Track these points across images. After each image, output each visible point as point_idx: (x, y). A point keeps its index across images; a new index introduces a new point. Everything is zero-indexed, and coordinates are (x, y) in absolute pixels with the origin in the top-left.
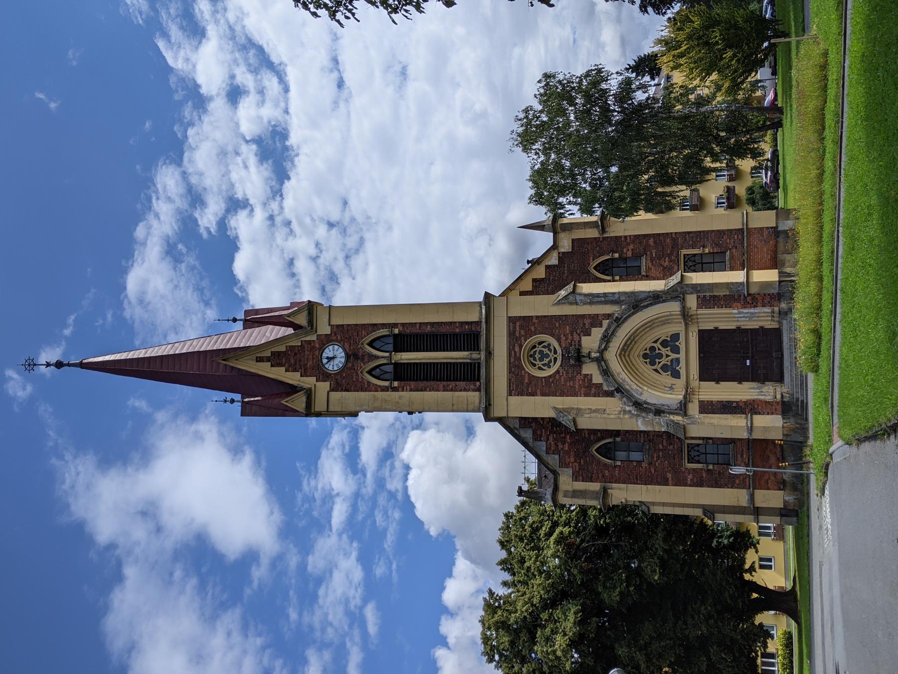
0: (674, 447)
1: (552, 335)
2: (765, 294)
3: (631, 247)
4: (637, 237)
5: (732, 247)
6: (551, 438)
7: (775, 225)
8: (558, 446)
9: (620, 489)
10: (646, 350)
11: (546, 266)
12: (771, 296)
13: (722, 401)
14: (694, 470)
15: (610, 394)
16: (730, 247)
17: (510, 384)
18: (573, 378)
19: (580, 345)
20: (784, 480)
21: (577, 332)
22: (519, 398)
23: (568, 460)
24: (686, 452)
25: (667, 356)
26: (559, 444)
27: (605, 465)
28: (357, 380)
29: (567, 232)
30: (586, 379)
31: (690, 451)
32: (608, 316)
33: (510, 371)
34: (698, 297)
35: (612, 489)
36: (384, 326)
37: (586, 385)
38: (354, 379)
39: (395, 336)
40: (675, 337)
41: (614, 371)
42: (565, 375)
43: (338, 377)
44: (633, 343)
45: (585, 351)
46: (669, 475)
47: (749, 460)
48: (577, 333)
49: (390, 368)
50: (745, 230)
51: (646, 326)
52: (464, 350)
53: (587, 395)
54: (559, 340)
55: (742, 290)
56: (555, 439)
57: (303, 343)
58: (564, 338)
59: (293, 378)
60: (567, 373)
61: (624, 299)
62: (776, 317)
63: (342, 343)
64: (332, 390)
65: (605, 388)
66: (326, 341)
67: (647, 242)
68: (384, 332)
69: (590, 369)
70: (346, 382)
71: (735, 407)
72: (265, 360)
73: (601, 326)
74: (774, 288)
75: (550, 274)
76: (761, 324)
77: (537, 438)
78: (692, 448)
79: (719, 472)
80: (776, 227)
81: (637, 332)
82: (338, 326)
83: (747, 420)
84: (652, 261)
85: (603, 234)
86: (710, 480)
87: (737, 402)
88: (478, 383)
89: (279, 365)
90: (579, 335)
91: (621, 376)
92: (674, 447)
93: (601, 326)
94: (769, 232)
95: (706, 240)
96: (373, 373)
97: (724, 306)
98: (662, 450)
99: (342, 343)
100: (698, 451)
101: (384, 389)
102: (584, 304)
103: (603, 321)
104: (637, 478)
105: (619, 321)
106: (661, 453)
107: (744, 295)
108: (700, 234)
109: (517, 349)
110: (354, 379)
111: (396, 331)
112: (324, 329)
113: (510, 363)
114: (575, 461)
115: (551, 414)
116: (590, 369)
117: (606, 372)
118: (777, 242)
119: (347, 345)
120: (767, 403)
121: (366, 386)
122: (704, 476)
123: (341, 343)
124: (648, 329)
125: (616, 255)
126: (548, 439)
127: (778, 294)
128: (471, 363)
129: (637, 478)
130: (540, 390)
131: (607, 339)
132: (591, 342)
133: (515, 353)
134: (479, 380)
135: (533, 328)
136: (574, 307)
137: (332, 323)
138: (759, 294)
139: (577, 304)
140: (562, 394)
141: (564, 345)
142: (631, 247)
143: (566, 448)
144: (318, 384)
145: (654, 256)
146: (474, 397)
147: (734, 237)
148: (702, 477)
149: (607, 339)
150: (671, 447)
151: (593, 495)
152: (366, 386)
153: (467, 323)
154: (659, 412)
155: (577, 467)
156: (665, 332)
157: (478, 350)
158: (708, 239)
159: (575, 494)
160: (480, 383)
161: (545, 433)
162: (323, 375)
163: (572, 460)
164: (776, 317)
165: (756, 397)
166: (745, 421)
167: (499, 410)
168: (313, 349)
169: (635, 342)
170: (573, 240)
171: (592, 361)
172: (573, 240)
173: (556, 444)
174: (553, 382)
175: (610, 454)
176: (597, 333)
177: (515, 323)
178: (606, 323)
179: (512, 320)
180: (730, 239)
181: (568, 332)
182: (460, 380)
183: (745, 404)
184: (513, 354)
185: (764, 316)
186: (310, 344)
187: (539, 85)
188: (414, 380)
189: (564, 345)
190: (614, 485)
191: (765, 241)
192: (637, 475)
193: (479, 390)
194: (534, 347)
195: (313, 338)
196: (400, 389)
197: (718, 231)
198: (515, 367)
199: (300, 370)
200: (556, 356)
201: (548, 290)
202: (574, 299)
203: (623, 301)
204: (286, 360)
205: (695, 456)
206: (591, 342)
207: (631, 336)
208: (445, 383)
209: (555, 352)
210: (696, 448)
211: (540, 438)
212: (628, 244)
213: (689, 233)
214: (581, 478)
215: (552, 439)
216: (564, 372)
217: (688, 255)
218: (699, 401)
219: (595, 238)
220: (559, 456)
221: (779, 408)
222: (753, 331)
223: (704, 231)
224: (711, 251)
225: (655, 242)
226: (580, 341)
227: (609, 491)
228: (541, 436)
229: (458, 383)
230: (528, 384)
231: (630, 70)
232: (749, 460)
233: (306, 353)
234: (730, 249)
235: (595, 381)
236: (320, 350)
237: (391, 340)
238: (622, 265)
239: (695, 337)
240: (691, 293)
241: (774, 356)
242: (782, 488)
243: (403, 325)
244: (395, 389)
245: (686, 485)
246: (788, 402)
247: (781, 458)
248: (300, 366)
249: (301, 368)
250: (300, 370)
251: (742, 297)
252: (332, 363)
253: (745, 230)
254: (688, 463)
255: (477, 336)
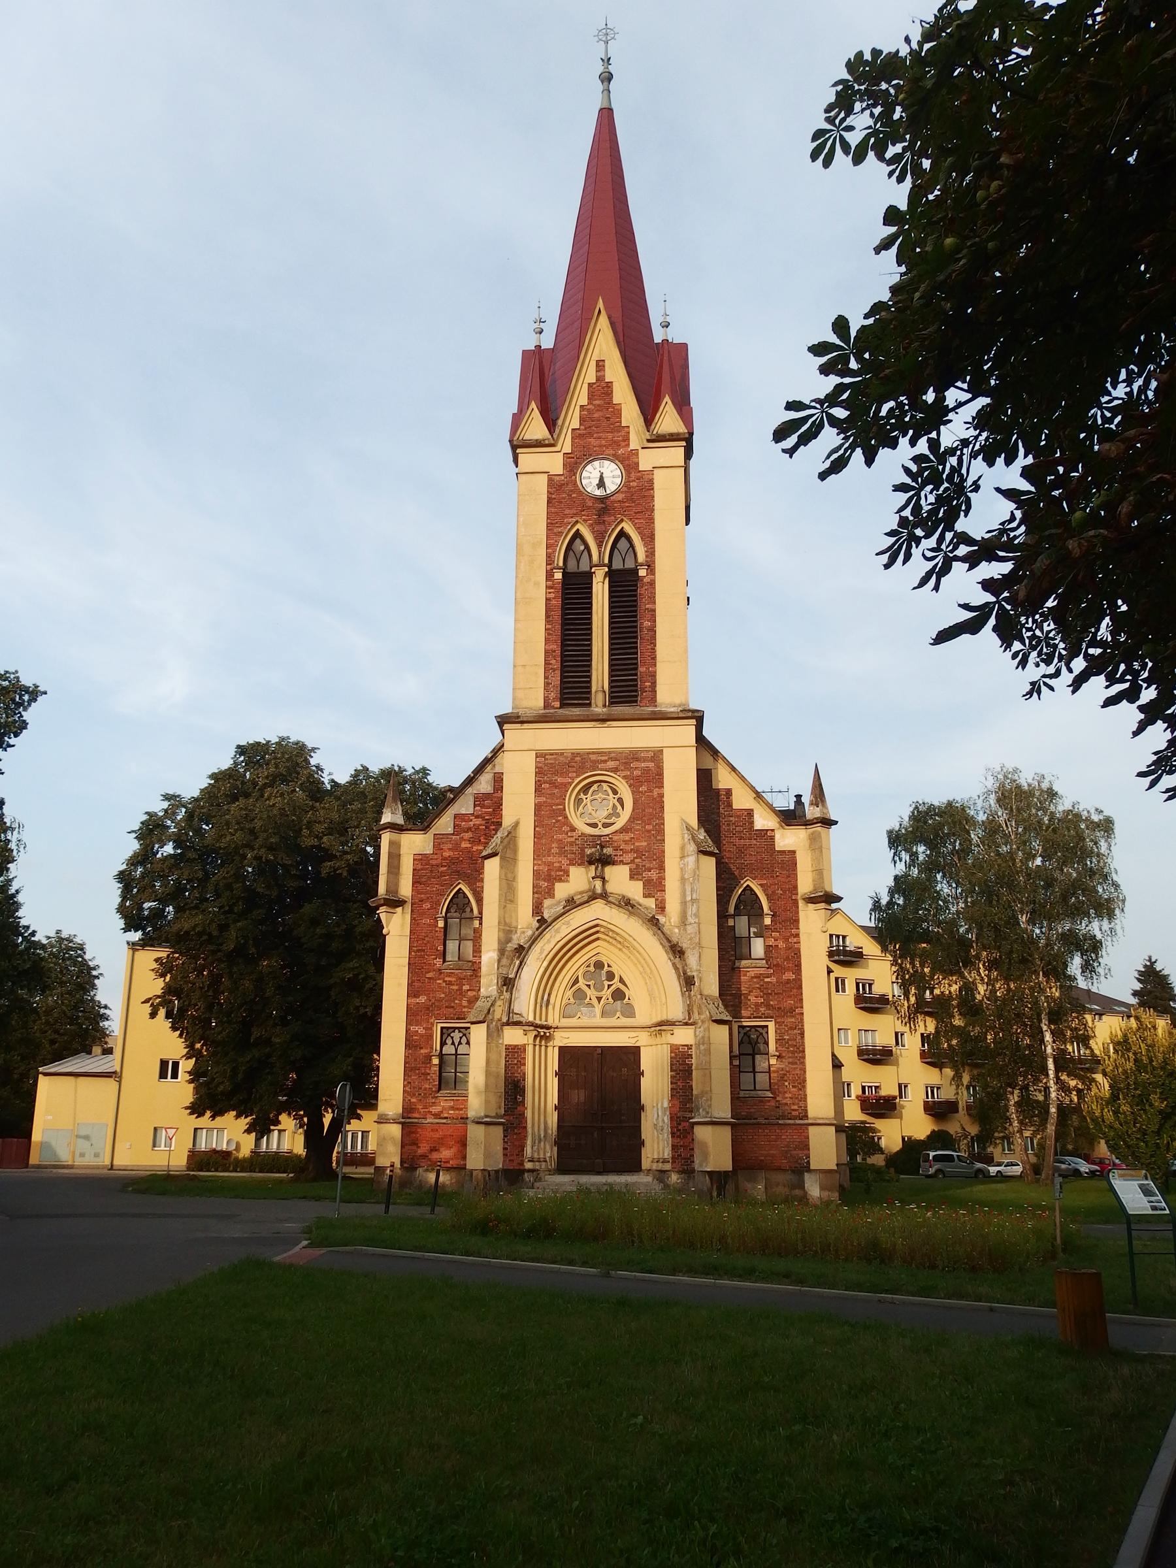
0: (465, 1007)
1: (632, 819)
2: (693, 1149)
3: (781, 944)
4: (797, 953)
5: (778, 1101)
6: (478, 821)
7: (812, 1167)
8: (467, 832)
9: (403, 925)
10: (609, 966)
11: (752, 810)
12: (690, 1159)
13: (524, 1080)
14: (430, 1037)
15: (537, 909)
16: (778, 1099)
17: (556, 754)
18: (562, 852)
19: (613, 863)
20: (416, 1169)
21: (636, 858)
22: (533, 770)
23: (445, 847)
24: (458, 1025)
25: (599, 999)
26: (469, 835)
27: (438, 903)
28: (566, 516)
29: (807, 844)
30: (561, 873)
31: (460, 1032)
32: (661, 908)
33: (575, 754)
34: (689, 1047)
35: (403, 913)
36: (651, 553)
37: (553, 873)
38: (567, 511)
39: (635, 571)
40: (629, 1012)
41: (571, 916)
42: (569, 840)
43: (570, 487)
44: (619, 946)
45: (609, 871)
46: (422, 999)
47: (446, 1118)
48: (634, 858)
49: (584, 567)
50: (806, 1122)
51: (645, 966)
52: (611, 682)
53: (537, 874)
54: (624, 830)
55: (699, 1115)
56: (477, 828)
57: (626, 429)
58: (627, 838)
59: (572, 420)
60: (571, 844)
61: (689, 932)
62: (658, 1166)
63: (625, 489)
64: (551, 479)
65: (547, 903)
66: (629, 463)
67: (788, 969)
68: (641, 557)
69: (579, 879)
70: (564, 498)
71: (516, 1098)
72: (599, 374)
73: (645, 896)
74: (701, 1165)
75: (739, 816)
76: (648, 1143)
77: (480, 800)
78: (465, 1035)
79: (429, 1074)
80: (809, 1170)
81: (635, 952)
82: (651, 481)
83: (494, 1117)
84: (758, 977)
85: (804, 899)
86: (415, 1060)
87: (523, 1102)
88: (557, 704)
89: (591, 397)
90: (632, 862)
91: (564, 927)
92: (465, 1007)
93: (645, 896)
94: (801, 1158)
95: (791, 1060)
96: (578, 541)
97: (674, 1086)
98: (460, 989)
99: (625, 489)
100: (460, 1043)
101: (550, 559)
102: (681, 869)
103: (654, 899)
104: (418, 951)
105: (653, 923)
106: (455, 987)
107: (692, 1118)
108: (800, 1052)
109: (611, 764)
110: (567, 511)
111: (642, 572)
112: (648, 459)
113: (589, 753)
114: (445, 859)
115: (507, 820)
116: (579, 879)
117: (571, 904)
118: (785, 1170)
119: (620, 497)
120: (522, 1148)
121: (555, 530)
122: (422, 1051)
123: (625, 487)
124: (641, 969)
125: (768, 921)
126: (477, 817)
127: (693, 1171)
128: (590, 693)
129: (418, 951)
130: (544, 802)
131: (627, 904)
132: (619, 879)
133: (605, 761)
134: (562, 706)
135: (643, 788)
136: (677, 853)
137: (656, 471)
138: (693, 1140)
139: (682, 857)
140: (537, 835)
141: (615, 838)
142: (781, 944)
143: (464, 845)
144: (560, 456)
145: (766, 980)
146: (535, 700)
147: (793, 1104)
148: (421, 1048)
149: (627, 904)
150: (465, 1003)
151: (393, 887)
152: (555, 530)
153: (654, 684)
154: (508, 983)
155: (434, 862)
156: (636, 993)
157: (611, 703)
158: (792, 1063)
159: (395, 857)
160: (557, 708)
161: (486, 813)
162: (574, 464)
163: (446, 854)
164: (658, 1166)
165: (529, 1130)
166: (494, 1114)
167: (516, 736)
168: (616, 444)
169: (620, 950)
170: (794, 852)
171: (590, 882)
172: (794, 852)
173: (469, 829)
174: (558, 821)
175: (456, 912)
176: (635, 890)
177: (653, 759)
178: (651, 903)
179: (656, 756)
180: (791, 1098)
181: (637, 844)
182: (562, 677)
183: (520, 1115)
184: (603, 758)
185: (658, 1148)
186: (624, 441)
187: (1092, 811)
188: (563, 604)
189: (615, 838)
190: (408, 917)
191: (786, 1152)
192: (424, 951)
193: (547, 705)
194: (615, 792)
195: (634, 444)
196: (550, 583)
197: (804, 1081)
198: (581, 762)
199: (582, 427)
200: (600, 826)
201: (713, 814)
202: (689, 853)
203: (685, 930)
204: (599, 405)
205: (452, 1038)
206: (619, 879)
207: (629, 942)
208: (558, 652)
209: (606, 825)
210: (464, 1040)
211: (479, 805)
212: (786, 939)
213: (802, 1034)
214: (419, 867)
215: (478, 823)
216: (573, 839)
217: (767, 1033)
218: (525, 1045)
219: (796, 887)
220: (453, 834)
221: (513, 1166)
222: (638, 1129)
223: (804, 1057)
224: (772, 1069)
225: (788, 982)
226: (622, 862)
227: (399, 910)
228: (483, 806)
229: (558, 673)
230: (553, 784)
231: (1148, 964)
232: (446, 1118)
233: (610, 436)
234: (774, 1098)
235: (559, 887)
236: (614, 455)
237: (630, 564)
238: (753, 930)
239: (628, 1040)
240: (695, 1036)
241: (597, 1160)
242: (405, 1165)
243: (652, 584)
244: (549, 575)
245: (409, 1023)
246: (523, 1180)
247: (449, 1165)
248: (590, 427)
249: (586, 429)
250: (582, 427)
251: (688, 1115)
252: (607, 482)
253: (806, 1122)
254: (442, 1028)
255: (632, 700)
